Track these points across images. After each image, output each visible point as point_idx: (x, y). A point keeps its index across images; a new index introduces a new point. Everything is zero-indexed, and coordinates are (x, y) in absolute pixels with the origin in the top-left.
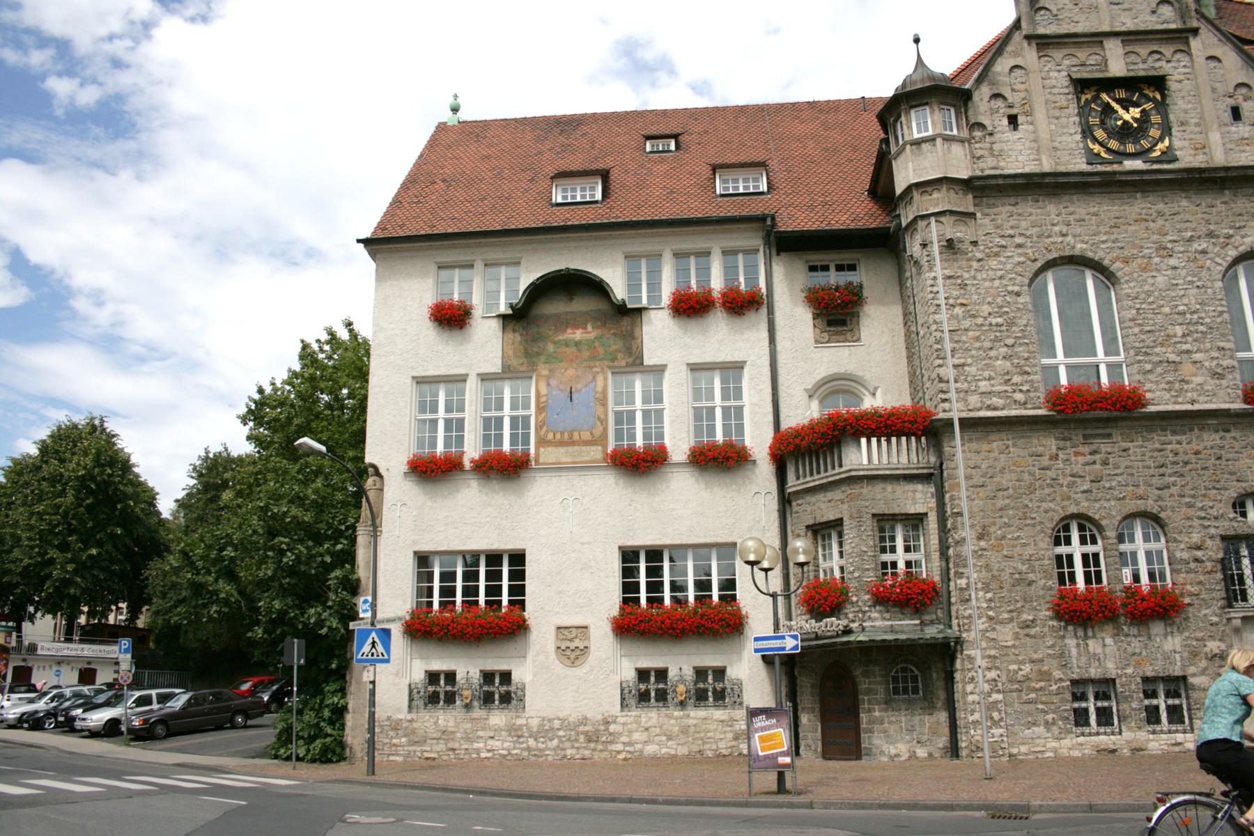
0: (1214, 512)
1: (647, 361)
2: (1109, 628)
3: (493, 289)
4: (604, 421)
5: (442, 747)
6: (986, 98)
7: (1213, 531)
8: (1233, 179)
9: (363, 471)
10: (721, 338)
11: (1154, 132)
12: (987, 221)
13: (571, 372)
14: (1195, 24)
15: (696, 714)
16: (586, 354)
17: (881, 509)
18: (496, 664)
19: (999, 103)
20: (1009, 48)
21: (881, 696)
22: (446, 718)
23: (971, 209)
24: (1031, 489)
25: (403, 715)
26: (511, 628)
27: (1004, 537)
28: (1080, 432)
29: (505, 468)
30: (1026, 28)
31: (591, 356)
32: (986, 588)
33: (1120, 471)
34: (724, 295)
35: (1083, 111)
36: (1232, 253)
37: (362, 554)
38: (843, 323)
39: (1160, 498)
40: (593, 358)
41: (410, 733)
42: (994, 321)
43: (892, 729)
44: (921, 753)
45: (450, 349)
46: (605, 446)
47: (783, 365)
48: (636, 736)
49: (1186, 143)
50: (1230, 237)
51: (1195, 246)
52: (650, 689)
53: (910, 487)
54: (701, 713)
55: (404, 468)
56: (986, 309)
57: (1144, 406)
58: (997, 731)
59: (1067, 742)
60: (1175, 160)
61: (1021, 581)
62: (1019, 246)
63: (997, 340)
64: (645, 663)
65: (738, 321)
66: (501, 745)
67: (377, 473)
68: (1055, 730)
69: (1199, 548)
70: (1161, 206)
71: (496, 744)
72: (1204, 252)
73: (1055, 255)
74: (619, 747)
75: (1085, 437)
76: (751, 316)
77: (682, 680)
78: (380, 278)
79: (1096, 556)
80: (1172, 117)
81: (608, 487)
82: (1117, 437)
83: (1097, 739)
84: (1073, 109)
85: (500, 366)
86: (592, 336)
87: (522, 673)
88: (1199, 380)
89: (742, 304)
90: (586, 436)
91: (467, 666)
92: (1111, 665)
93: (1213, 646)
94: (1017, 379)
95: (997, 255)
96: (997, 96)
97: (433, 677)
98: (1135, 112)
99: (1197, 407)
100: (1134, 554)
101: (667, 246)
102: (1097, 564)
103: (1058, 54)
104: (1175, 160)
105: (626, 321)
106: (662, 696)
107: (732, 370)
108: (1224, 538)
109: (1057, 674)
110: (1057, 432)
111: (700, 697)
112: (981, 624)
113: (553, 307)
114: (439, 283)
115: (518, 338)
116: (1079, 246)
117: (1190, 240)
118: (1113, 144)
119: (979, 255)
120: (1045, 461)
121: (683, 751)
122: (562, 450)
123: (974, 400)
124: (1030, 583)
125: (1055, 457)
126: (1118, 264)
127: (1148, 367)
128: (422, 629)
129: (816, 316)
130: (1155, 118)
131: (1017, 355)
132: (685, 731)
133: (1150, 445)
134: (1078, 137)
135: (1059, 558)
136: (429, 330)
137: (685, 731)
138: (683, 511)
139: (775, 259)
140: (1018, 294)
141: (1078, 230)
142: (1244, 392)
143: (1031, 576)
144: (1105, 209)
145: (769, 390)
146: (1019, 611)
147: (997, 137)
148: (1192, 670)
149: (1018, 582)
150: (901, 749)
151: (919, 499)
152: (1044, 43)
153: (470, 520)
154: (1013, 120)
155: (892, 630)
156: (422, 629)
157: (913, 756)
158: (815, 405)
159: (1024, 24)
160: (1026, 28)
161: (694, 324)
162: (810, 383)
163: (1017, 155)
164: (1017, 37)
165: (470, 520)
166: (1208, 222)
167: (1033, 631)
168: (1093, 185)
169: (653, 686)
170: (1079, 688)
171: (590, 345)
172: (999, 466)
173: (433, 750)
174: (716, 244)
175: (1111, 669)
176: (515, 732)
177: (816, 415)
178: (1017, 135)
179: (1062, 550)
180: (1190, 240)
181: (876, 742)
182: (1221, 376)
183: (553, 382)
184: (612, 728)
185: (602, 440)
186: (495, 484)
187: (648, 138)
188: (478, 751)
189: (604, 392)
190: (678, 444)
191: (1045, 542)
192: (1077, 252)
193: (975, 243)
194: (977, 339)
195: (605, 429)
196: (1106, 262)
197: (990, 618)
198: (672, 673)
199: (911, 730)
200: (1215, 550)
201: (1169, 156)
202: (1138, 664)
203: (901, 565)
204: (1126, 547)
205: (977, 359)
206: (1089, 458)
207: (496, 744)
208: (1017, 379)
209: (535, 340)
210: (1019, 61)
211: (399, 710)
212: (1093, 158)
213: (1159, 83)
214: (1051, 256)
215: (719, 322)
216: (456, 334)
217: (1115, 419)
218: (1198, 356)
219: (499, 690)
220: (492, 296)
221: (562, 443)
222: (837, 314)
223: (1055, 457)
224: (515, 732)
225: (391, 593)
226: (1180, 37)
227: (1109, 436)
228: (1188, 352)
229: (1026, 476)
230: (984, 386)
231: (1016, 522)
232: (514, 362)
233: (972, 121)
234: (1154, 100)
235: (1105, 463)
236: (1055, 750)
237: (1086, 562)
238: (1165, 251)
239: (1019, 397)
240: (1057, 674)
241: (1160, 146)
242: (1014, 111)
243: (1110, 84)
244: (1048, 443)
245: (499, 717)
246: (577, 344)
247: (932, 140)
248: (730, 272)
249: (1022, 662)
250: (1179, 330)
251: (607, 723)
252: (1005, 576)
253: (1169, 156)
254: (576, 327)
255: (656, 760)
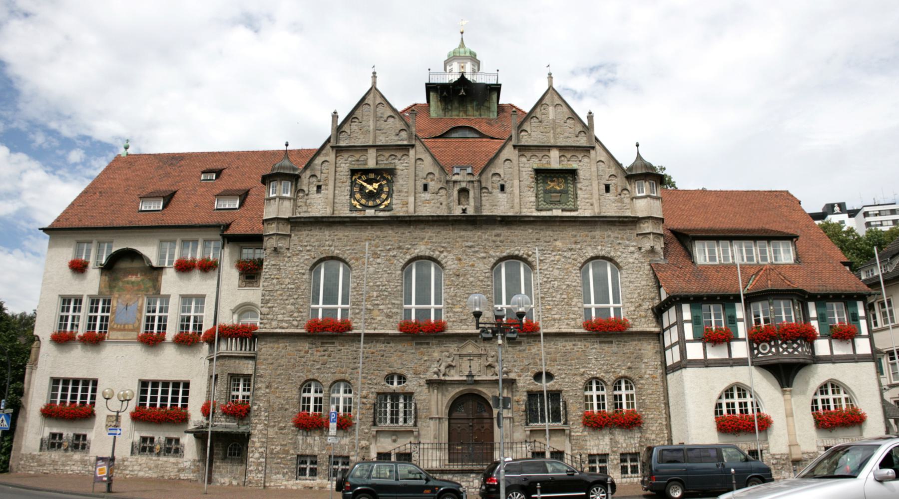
0: (375, 381)
1: (162, 293)
2: (318, 432)
3: (96, 256)
4: (140, 321)
5: (51, 468)
6: (308, 176)
7: (373, 390)
8: (415, 221)
9: (34, 339)
10: (197, 284)
11: (384, 196)
12: (296, 238)
13: (128, 296)
14: (413, 143)
15: (163, 459)
16: (136, 288)
17: (232, 371)
18: (173, 435)
19: (314, 179)
20: (324, 152)
21: (220, 456)
22: (55, 455)
23: (289, 233)
24: (294, 366)
25: (37, 452)
26: (86, 415)
27: (277, 388)
28: (320, 341)
29: (93, 341)
30: (333, 143)
31: (138, 289)
32: (265, 411)
33: (335, 359)
34: (200, 262)
35: (353, 183)
36: (408, 257)
37: (27, 377)
38: (253, 278)
39: (351, 373)
40: (138, 290)
41: (39, 461)
42: (290, 286)
43: (224, 471)
44: (235, 483)
45: (77, 282)
46: (138, 332)
47: (224, 297)
48: (136, 468)
49: (399, 202)
50: (408, 249)
51: (391, 253)
52: (145, 447)
53: (246, 362)
54: (165, 459)
55: (49, 338)
56: (288, 280)
57: (350, 329)
58: (260, 475)
59: (291, 482)
60: (391, 210)
61: (282, 409)
62: (308, 251)
63: (290, 295)
64: (145, 434)
65: (205, 275)
66: (77, 469)
67: (39, 340)
68: (287, 477)
69: (365, 398)
70: (378, 233)
71: (75, 468)
72: (394, 256)
73: (324, 255)
74: (128, 472)
75: (322, 343)
76: (211, 273)
77: (159, 443)
78: (50, 246)
79: (632, 395)
80: (394, 188)
81: (136, 352)
82: (337, 344)
83: (307, 481)
84: (348, 183)
85: (97, 290)
86: (139, 279)
87: (91, 436)
88: (379, 318)
89: (208, 267)
90: (131, 327)
91: (68, 432)
92: (316, 449)
93: (364, 443)
94: (296, 315)
95: (297, 255)
96: (314, 176)
97: (144, 439)
98: (376, 185)
99: (376, 332)
100: (338, 399)
101: (179, 236)
102: (603, 400)
103: (346, 155)
104: (391, 210)
105: (155, 273)
106: (151, 450)
107: (200, 299)
108: (378, 394)
109: (292, 452)
110: (310, 340)
111: (168, 451)
112: (260, 427)
113: (124, 265)
114: (78, 251)
115: (107, 278)
116: (337, 251)
117: (389, 250)
118: (363, 201)
119: (289, 255)
120: (302, 354)
121: (155, 475)
122: (119, 333)
123: (274, 323)
124: (286, 410)
125: (307, 352)
126: (353, 261)
127: (357, 311)
128: (49, 413)
129: (241, 274)
130: (386, 189)
131: (297, 303)
132: (157, 466)
133: (351, 348)
134: (348, 197)
135: (616, 396)
136: (67, 272)
137: (157, 466)
138: (170, 364)
139: (226, 244)
140: (303, 274)
141: (337, 244)
142: (400, 325)
143: (287, 407)
144: (351, 234)
145: (214, 309)
146: (279, 422)
147: (310, 196)
148: (352, 453)
149: (280, 409)
150: (226, 480)
151: (247, 368)
152: (339, 150)
153: (76, 363)
154: (319, 188)
155: (226, 427)
156: (49, 413)
157: (231, 484)
158: (236, 317)
159: (332, 140)
160: (333, 143)
161: (185, 276)
162: (233, 306)
163: (318, 206)
164: (328, 146)
165: (76, 363)
166: (400, 241)
167: (284, 432)
168: (347, 222)
169: (148, 443)
170: (302, 459)
171: (138, 283)
172: (281, 355)
173: (47, 469)
174: (201, 236)
175: (316, 450)
176: (84, 462)
177: (235, 322)
178: (320, 195)
179: (617, 393)
180: (389, 250)
181: (216, 476)
182: (391, 317)
183: (120, 301)
184: (126, 463)
185: (138, 329)
186: (89, 348)
187: (203, 172)
188: (67, 470)
189: (142, 307)
190: (172, 331)
191: (295, 392)
192: (335, 255)
193: (288, 249)
194: (281, 295)
195: (140, 324)
196: (347, 260)
197: (265, 425)
198: (156, 439)
199: (232, 472)
200: (372, 399)
201: (388, 208)
202: (328, 449)
203: (240, 398)
204: (335, 395)
205: (280, 304)
206: (323, 353)
207: (75, 468)
208: (296, 315)
209: (114, 280)
210: (327, 158)
211: (35, 450)
212: (353, 208)
213: (392, 172)
214: (322, 256)
215: (196, 275)
216: (81, 275)
217: (336, 336)
218: (381, 307)
219: (80, 443)
220: (98, 256)
221: (120, 330)
222: (250, 273)
223: (307, 352)
224: (84, 462)
225: (38, 393)
226: (405, 148)
227: (333, 343)
228: (377, 305)
229: (292, 360)
230: (280, 317)
231: (285, 381)
232: (104, 290)
233: (299, 188)
234: (387, 180)
235: (329, 356)
236: (285, 485)
237: (627, 398)
238: (376, 255)
239: (295, 323)
240: (292, 452)
241: (386, 203)
242: (320, 184)
243: (366, 172)
244: (305, 346)
245: (77, 456)
246: (133, 283)
247: (274, 198)
248: (203, 252)
249: (277, 445)
250: (375, 294)
251: (124, 461)
252: (275, 406)
253: (388, 208)
254: (133, 275)
255: (148, 480)
